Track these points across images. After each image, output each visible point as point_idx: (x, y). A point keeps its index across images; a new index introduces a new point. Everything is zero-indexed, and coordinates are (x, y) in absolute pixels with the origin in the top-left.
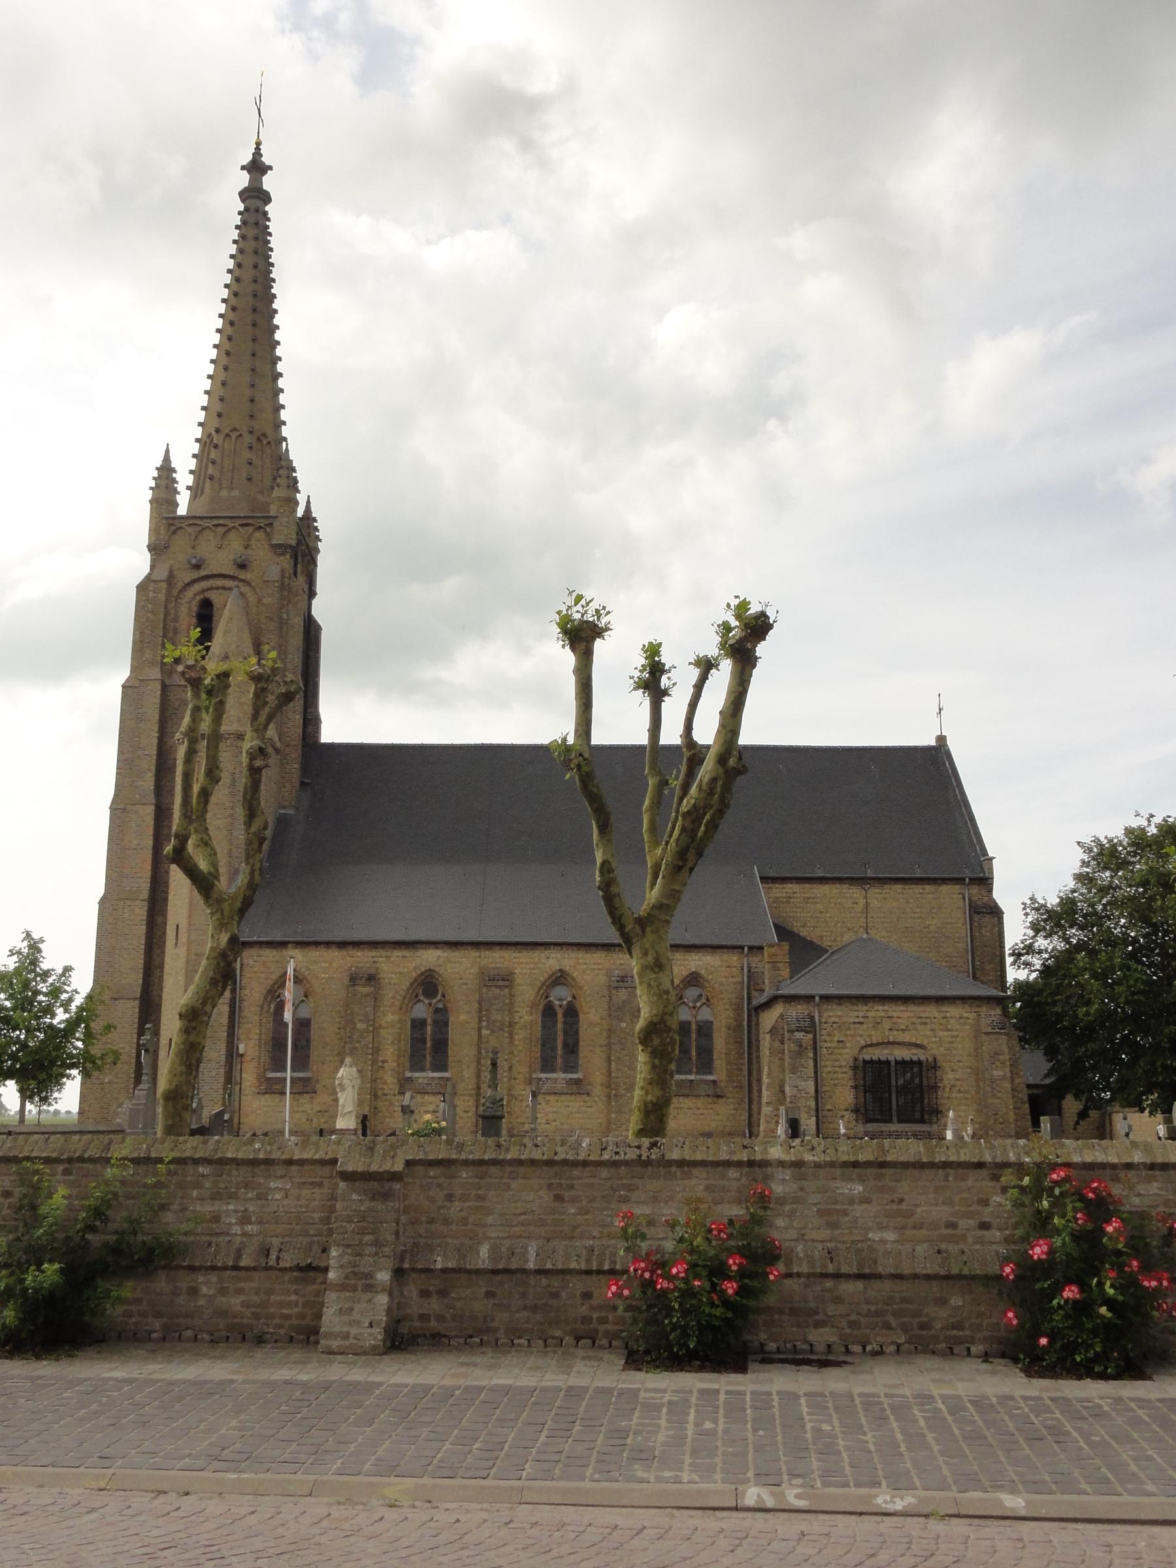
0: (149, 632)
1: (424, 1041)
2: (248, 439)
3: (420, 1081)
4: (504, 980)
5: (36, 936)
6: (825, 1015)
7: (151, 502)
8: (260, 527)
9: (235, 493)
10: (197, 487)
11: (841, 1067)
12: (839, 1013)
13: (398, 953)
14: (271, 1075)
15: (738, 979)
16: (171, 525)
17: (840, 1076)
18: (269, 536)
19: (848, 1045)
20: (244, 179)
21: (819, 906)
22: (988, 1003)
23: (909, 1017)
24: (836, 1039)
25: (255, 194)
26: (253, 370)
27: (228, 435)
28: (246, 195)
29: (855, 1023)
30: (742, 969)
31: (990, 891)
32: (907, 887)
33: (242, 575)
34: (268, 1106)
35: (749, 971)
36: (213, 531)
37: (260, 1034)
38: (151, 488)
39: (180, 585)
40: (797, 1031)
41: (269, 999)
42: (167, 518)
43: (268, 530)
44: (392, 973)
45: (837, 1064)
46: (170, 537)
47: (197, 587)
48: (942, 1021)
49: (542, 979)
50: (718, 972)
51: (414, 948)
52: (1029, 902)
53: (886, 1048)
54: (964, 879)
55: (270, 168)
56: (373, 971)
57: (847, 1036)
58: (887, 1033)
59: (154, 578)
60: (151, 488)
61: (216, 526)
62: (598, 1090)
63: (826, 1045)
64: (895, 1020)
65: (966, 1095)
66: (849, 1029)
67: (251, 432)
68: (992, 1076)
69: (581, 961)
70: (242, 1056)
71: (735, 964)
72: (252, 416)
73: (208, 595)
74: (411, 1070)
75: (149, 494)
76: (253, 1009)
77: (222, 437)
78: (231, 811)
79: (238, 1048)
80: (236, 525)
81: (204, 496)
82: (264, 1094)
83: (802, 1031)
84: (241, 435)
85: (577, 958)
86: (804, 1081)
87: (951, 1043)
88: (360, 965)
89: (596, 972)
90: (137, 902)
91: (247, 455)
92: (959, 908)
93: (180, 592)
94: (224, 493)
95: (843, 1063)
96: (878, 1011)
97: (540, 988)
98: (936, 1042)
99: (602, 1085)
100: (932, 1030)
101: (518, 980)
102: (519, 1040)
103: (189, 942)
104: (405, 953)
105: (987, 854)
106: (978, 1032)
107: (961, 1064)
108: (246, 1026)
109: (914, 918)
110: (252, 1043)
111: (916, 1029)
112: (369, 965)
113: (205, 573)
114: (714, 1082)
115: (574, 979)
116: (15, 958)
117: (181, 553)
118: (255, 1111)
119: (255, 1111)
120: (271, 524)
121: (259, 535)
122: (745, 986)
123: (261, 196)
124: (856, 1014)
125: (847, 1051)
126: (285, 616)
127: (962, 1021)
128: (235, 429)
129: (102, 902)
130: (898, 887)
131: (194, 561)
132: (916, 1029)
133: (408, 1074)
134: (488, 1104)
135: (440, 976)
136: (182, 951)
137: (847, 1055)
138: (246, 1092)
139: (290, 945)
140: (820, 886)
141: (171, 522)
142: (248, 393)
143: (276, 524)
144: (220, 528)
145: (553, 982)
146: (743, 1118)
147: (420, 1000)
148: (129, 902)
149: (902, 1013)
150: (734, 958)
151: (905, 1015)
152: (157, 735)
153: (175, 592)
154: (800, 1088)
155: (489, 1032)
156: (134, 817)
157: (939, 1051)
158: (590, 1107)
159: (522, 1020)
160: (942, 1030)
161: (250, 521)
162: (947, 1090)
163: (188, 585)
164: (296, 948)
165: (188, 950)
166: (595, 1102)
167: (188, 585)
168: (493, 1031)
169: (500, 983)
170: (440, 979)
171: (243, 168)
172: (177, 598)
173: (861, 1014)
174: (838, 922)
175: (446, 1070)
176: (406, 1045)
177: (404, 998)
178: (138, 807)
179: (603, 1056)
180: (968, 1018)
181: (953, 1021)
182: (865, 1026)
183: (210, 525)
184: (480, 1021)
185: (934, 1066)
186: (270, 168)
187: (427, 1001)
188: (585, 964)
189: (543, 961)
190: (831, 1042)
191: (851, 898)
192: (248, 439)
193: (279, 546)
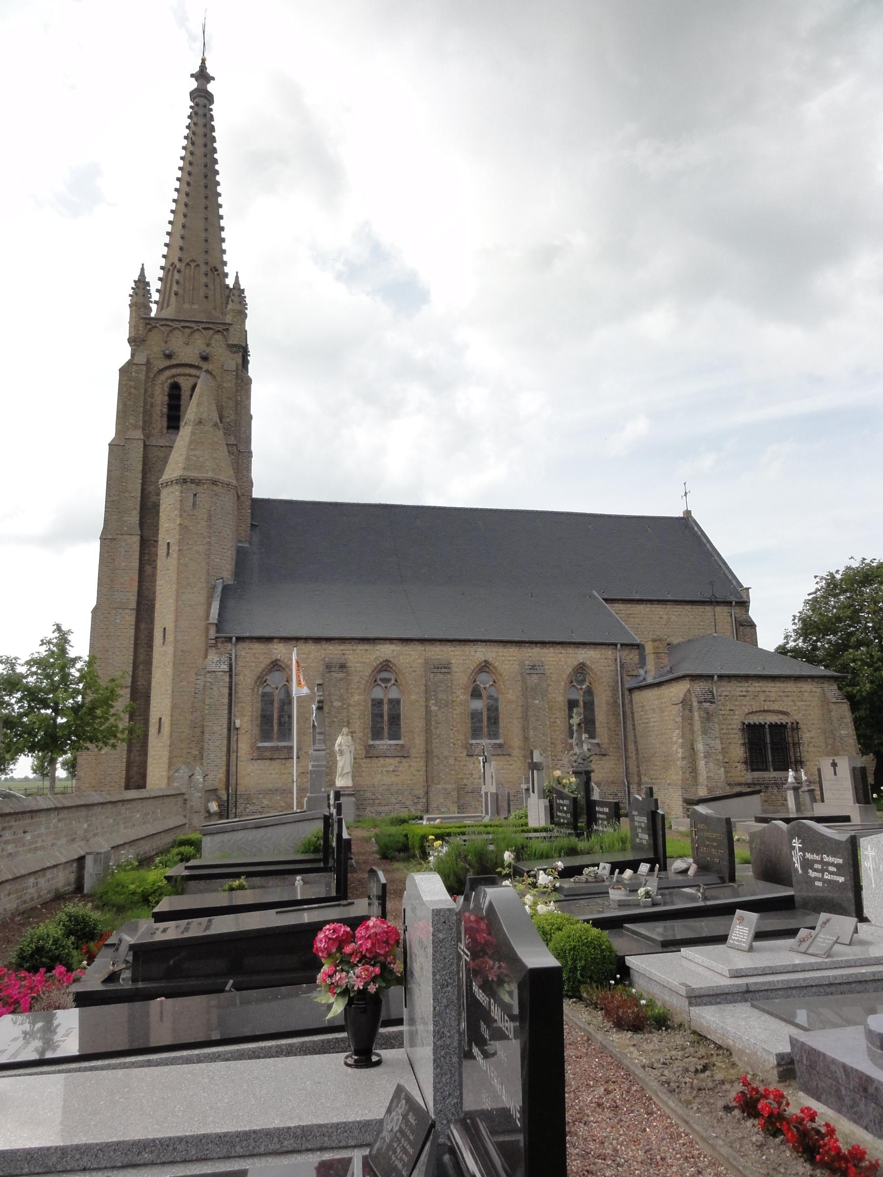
0: (132, 403)
1: (382, 716)
2: (203, 268)
3: (381, 747)
4: (444, 668)
5: (64, 628)
6: (720, 690)
7: (130, 306)
8: (219, 331)
9: (195, 307)
10: (163, 302)
11: (732, 729)
12: (729, 689)
13: (361, 647)
14: (260, 745)
15: (612, 668)
16: (147, 324)
17: (733, 736)
18: (226, 338)
19: (737, 712)
20: (194, 84)
21: (637, 620)
22: (829, 681)
23: (776, 692)
24: (728, 708)
25: (203, 94)
26: (206, 219)
27: (188, 264)
28: (195, 95)
29: (740, 696)
30: (616, 660)
31: (748, 611)
32: (694, 607)
33: (205, 366)
34: (260, 770)
35: (621, 662)
36: (181, 331)
37: (252, 712)
38: (130, 296)
39: (155, 370)
40: (705, 702)
41: (258, 684)
42: (144, 319)
43: (225, 333)
44: (357, 663)
45: (730, 727)
46: (147, 333)
47: (168, 373)
48: (799, 694)
49: (472, 668)
50: (598, 662)
51: (374, 643)
52: (798, 615)
53: (761, 715)
54: (732, 602)
55: (213, 79)
56: (342, 661)
57: (735, 705)
58: (762, 703)
59: (135, 361)
60: (130, 296)
61: (184, 327)
62: (516, 752)
63: (721, 712)
64: (768, 693)
65: (819, 749)
66: (736, 700)
67: (207, 263)
68: (841, 734)
69: (500, 654)
70: (237, 729)
71: (610, 657)
72: (207, 252)
73: (176, 379)
74: (373, 739)
75: (128, 301)
76: (245, 691)
77: (183, 265)
78: (209, 540)
79: (234, 723)
80: (200, 328)
81: (169, 308)
82: (256, 760)
83: (708, 702)
84: (198, 265)
85: (497, 652)
86: (713, 740)
87: (806, 710)
88: (331, 656)
89: (511, 662)
90: (127, 611)
91: (204, 280)
92: (727, 622)
93: (155, 376)
94: (186, 306)
95: (735, 726)
96: (755, 687)
97: (471, 674)
98: (795, 710)
99: (519, 748)
100: (793, 701)
101: (455, 669)
102: (457, 714)
103: (176, 641)
104: (367, 647)
105: (742, 586)
106: (825, 701)
107: (814, 726)
108: (240, 705)
109: (699, 629)
110: (246, 719)
111: (782, 700)
112: (338, 656)
113: (175, 362)
114: (598, 744)
115: (495, 668)
116: (44, 647)
117: (156, 344)
118: (249, 774)
119: (249, 774)
120: (227, 329)
121: (218, 337)
122: (619, 673)
123: (208, 96)
124: (740, 689)
125: (737, 717)
126: (239, 398)
127: (812, 694)
128: (194, 261)
129: (95, 611)
130: (688, 607)
131: (167, 352)
132: (782, 700)
133: (371, 742)
134: (580, 761)
135: (395, 666)
136: (170, 649)
137: (736, 720)
138: (242, 759)
139: (275, 640)
140: (638, 606)
141: (148, 321)
142: (203, 235)
143: (231, 329)
144: (186, 330)
145: (480, 669)
146: (621, 770)
147: (378, 685)
148: (120, 611)
149: (772, 688)
150: (609, 653)
151: (774, 689)
152: (140, 481)
153: (152, 375)
154: (711, 745)
155: (437, 708)
156: (123, 544)
157: (797, 717)
158: (511, 765)
159: (458, 699)
160: (800, 701)
161: (211, 326)
162: (806, 745)
163: (161, 371)
164: (280, 643)
165: (175, 647)
166: (515, 761)
167: (161, 371)
168: (440, 707)
169: (444, 670)
170: (394, 668)
171: (192, 76)
172: (153, 379)
173: (744, 689)
174: (650, 631)
175: (399, 739)
176: (368, 719)
177: (367, 682)
178: (126, 537)
179: (520, 726)
180: (816, 692)
181: (806, 694)
182: (747, 698)
183: (179, 326)
184: (427, 700)
185: (796, 727)
186: (213, 79)
187: (383, 685)
188: (504, 656)
189: (472, 654)
190: (724, 710)
191: (658, 614)
192: (203, 268)
193: (235, 346)
